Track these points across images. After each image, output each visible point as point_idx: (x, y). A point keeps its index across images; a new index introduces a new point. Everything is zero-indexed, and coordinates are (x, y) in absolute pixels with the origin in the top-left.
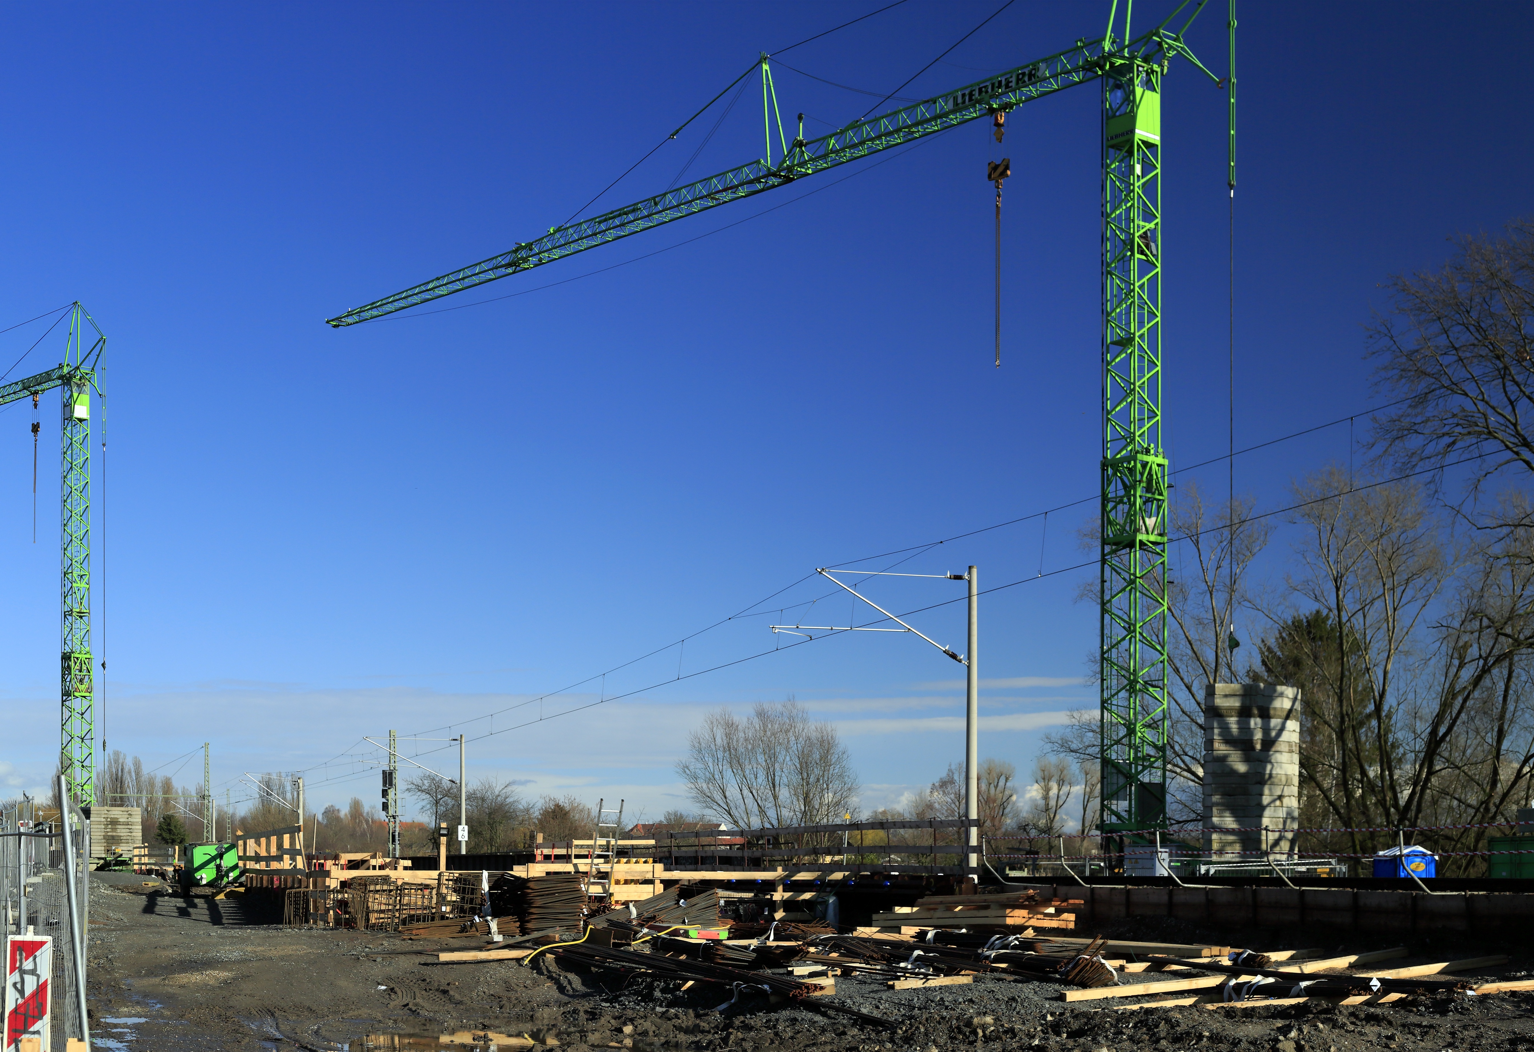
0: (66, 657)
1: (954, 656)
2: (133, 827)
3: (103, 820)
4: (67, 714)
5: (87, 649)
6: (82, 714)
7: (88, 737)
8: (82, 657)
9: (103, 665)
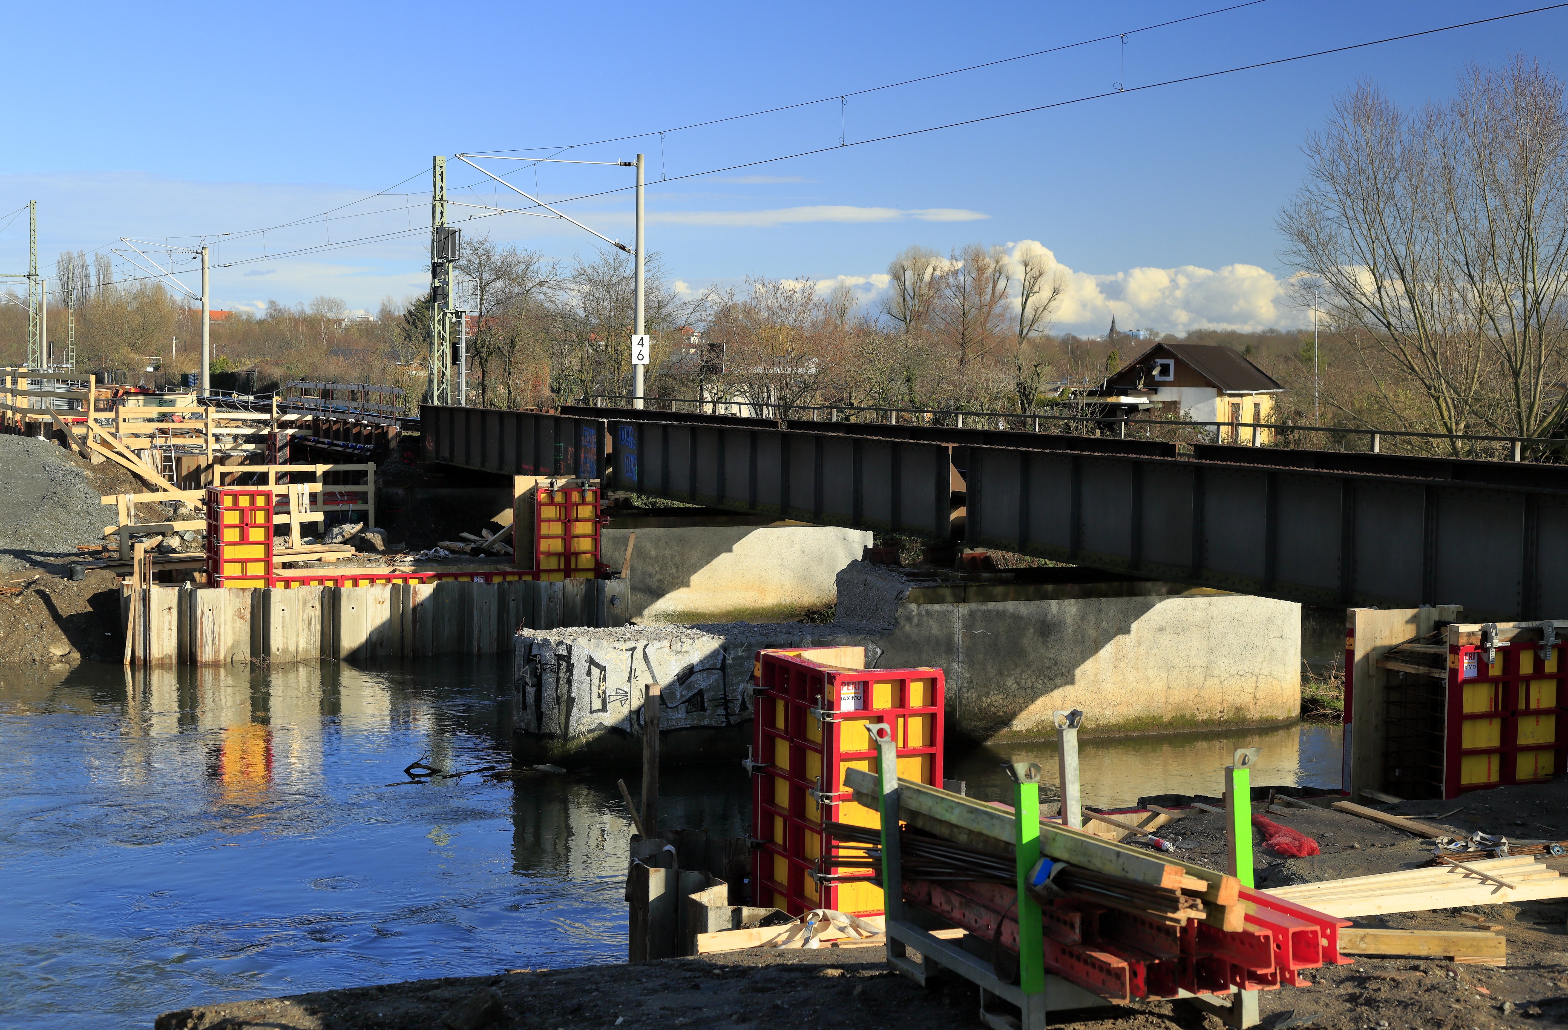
1: (623, 248)
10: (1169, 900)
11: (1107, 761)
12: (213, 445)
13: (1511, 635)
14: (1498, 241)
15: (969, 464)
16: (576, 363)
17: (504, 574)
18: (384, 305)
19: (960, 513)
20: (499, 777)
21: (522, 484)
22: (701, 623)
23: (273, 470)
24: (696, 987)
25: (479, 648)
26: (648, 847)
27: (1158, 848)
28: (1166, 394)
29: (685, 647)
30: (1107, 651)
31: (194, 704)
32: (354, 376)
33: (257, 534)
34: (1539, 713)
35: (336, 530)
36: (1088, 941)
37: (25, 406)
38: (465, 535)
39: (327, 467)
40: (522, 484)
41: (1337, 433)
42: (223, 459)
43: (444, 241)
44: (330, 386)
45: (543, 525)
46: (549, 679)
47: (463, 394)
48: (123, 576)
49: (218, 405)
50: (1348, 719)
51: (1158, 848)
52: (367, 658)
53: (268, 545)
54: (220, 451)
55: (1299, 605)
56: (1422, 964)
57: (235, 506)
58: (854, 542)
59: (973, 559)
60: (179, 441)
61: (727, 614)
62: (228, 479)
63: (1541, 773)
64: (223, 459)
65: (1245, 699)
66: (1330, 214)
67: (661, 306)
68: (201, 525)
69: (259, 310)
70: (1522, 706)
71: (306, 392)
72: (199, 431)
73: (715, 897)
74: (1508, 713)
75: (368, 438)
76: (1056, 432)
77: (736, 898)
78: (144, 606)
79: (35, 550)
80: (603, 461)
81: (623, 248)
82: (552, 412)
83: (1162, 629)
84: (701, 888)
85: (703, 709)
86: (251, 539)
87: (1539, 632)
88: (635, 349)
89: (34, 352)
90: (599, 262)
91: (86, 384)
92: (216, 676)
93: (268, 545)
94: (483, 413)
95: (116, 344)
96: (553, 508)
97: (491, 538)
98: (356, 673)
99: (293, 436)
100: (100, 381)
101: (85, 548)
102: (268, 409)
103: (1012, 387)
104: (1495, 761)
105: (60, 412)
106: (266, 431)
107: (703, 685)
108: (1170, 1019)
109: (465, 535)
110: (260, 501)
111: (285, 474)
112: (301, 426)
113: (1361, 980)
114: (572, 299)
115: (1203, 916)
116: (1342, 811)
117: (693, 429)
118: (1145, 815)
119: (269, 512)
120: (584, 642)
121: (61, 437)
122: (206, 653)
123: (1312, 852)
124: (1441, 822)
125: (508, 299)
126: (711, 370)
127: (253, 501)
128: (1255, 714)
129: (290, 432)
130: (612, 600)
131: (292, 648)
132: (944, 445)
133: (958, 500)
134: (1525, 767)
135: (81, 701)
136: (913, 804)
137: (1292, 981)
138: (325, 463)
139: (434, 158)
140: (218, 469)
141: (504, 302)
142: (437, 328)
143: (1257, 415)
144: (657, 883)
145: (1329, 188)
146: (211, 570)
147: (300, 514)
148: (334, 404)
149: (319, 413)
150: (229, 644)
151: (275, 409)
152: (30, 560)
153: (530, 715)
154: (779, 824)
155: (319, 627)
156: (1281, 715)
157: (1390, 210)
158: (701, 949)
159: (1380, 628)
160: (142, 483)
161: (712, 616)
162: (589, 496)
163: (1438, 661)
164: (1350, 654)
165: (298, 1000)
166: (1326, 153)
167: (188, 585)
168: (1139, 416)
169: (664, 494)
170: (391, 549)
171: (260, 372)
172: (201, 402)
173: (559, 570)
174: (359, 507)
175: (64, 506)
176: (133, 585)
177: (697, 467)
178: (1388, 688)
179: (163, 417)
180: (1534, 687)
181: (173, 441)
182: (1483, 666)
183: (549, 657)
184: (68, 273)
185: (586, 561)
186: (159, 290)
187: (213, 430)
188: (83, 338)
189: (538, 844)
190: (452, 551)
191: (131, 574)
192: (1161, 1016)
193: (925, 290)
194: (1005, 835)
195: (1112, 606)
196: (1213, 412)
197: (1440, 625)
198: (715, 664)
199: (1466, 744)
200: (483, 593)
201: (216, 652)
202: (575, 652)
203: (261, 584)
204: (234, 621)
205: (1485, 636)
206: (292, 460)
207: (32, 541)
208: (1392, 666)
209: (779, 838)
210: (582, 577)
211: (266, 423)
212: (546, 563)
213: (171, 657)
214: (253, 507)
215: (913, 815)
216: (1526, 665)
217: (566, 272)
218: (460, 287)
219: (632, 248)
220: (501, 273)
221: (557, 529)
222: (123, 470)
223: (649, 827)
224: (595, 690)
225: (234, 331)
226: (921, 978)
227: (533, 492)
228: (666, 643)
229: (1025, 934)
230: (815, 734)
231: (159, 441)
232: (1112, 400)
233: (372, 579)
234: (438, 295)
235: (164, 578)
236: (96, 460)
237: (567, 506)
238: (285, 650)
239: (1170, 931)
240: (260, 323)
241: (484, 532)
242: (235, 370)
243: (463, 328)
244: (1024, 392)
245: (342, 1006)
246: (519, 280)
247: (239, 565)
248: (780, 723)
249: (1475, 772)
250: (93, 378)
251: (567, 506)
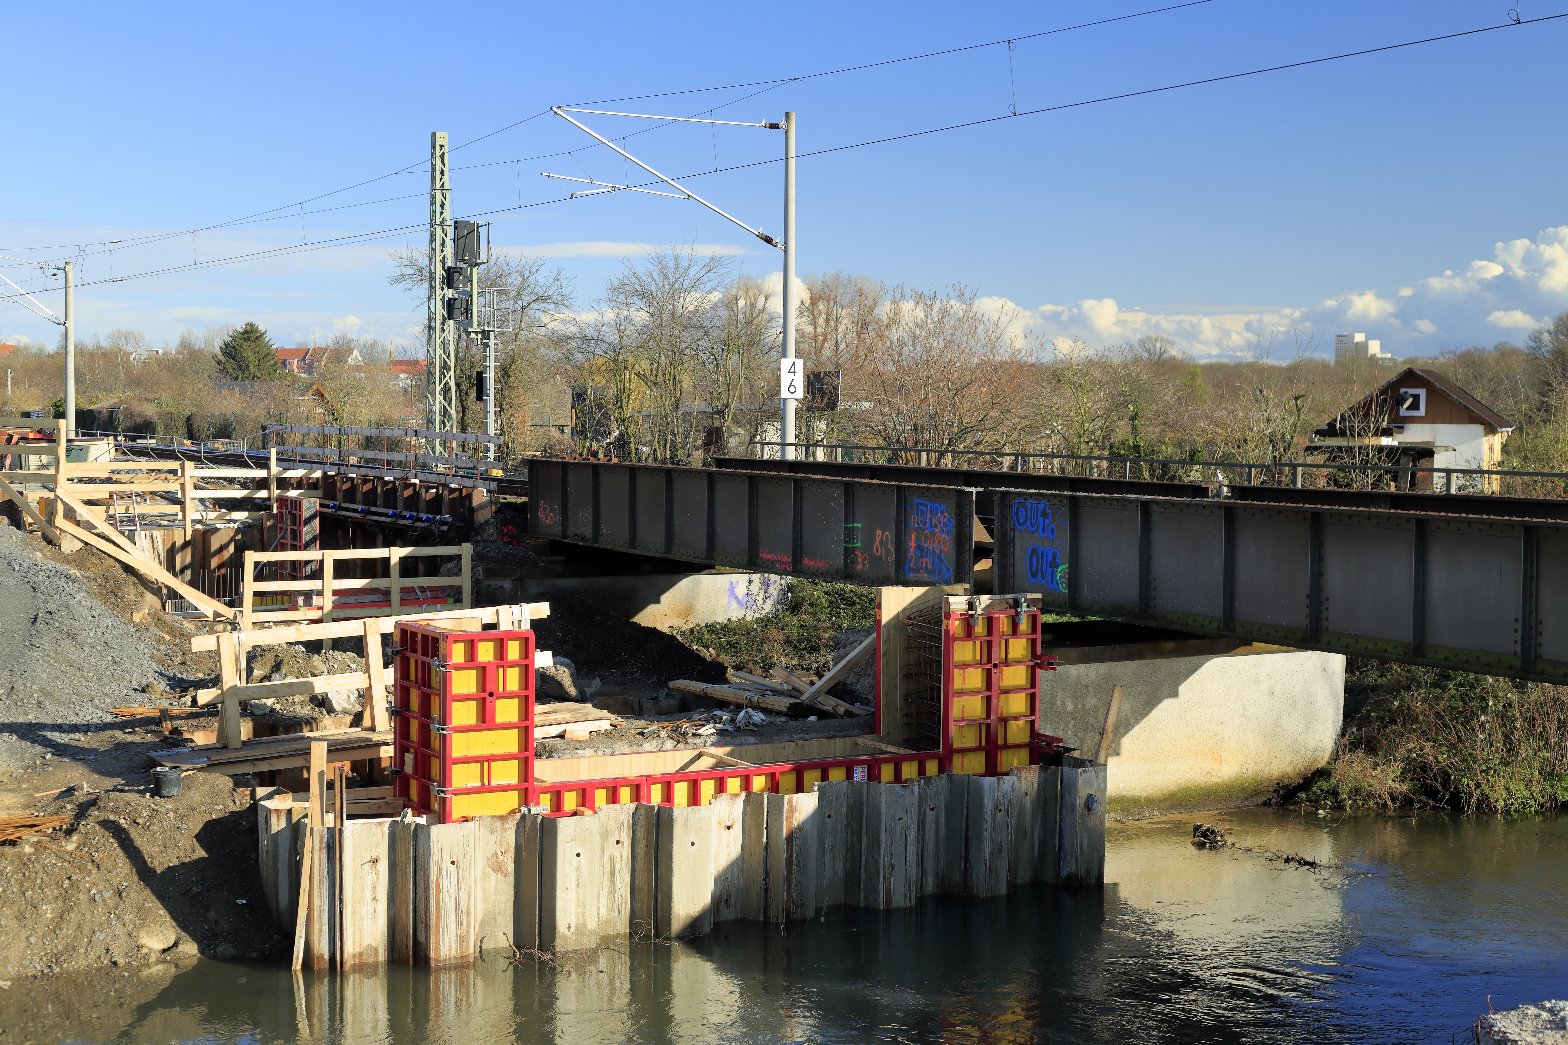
1: (768, 240)
18: (183, 337)
25: (889, 899)
39: (405, 551)
45: (957, 674)
54: (200, 521)
78: (331, 859)
79: (48, 720)
81: (768, 240)
86: (499, 719)
88: (786, 379)
92: (462, 984)
96: (969, 644)
132: (967, 489)
133: (982, 552)
139: (434, 135)
149: (327, 467)
150: (479, 919)
152: (48, 744)
155: (627, 879)
164: (880, 621)
171: (125, 409)
175: (71, 636)
204: (485, 876)
207: (39, 704)
211: (263, 484)
213: (376, 950)
221: (974, 678)
222: (109, 562)
225: (101, 363)
230: (435, 682)
236: (69, 546)
238: (581, 929)
240: (50, 356)
242: (93, 407)
247: (475, 767)
248: (413, 676)
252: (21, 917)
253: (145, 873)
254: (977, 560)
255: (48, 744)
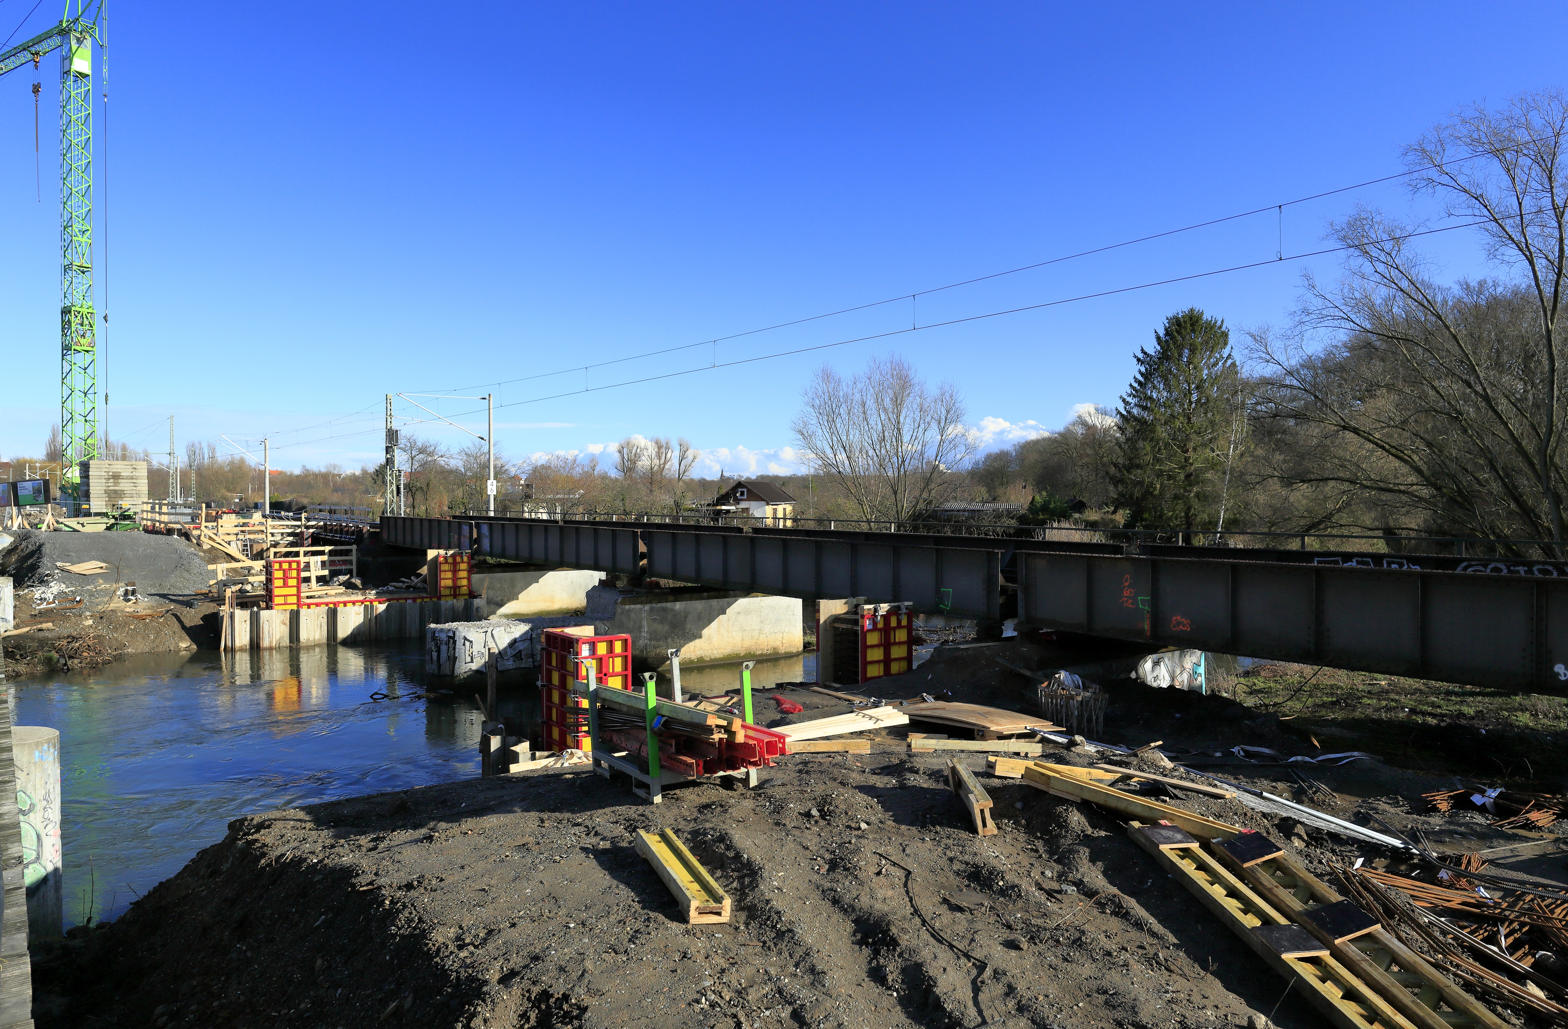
0: (66, 311)
1: (482, 439)
2: (138, 481)
3: (104, 474)
4: (67, 368)
5: (90, 304)
6: (85, 369)
7: (91, 391)
8: (84, 311)
9: (105, 318)
10: (709, 730)
11: (715, 676)
12: (270, 538)
13: (886, 609)
14: (886, 434)
15: (648, 538)
16: (461, 495)
17: (423, 598)
19: (644, 562)
20: (419, 697)
21: (431, 554)
22: (521, 618)
23: (302, 550)
24: (503, 788)
26: (490, 726)
27: (732, 713)
28: (743, 505)
29: (512, 630)
30: (714, 624)
31: (259, 669)
32: (346, 502)
33: (293, 582)
34: (900, 643)
35: (335, 579)
36: (679, 752)
37: (166, 520)
38: (403, 579)
40: (431, 554)
41: (820, 521)
42: (276, 545)
43: (392, 436)
44: (333, 507)
46: (444, 648)
47: (402, 510)
48: (220, 605)
49: (273, 518)
50: (818, 650)
51: (732, 713)
52: (351, 642)
53: (298, 587)
55: (800, 601)
56: (833, 755)
57: (281, 568)
58: (593, 577)
59: (651, 582)
60: (252, 537)
61: (535, 614)
62: (278, 555)
63: (902, 670)
64: (276, 545)
65: (778, 644)
66: (812, 422)
67: (502, 466)
68: (263, 578)
69: (297, 471)
70: (892, 641)
71: (320, 511)
72: (263, 531)
73: (522, 748)
74: (886, 645)
75: (353, 533)
76: (692, 523)
77: (534, 748)
80: (473, 542)
81: (482, 439)
82: (448, 518)
83: (739, 613)
84: (516, 744)
85: (522, 659)
87: (899, 608)
89: (173, 492)
90: (471, 445)
91: (201, 509)
92: (271, 655)
93: (298, 587)
94: (412, 519)
95: (216, 488)
97: (416, 581)
98: (345, 649)
99: (313, 533)
100: (208, 506)
101: (199, 592)
102: (300, 519)
103: (672, 503)
104: (882, 666)
105: (186, 523)
106: (298, 531)
107: (521, 648)
108: (719, 785)
109: (403, 579)
110: (294, 565)
111: (309, 552)
112: (317, 527)
113: (805, 763)
114: (456, 463)
115: (726, 736)
116: (814, 691)
117: (516, 525)
118: (728, 698)
119: (299, 570)
120: (464, 629)
121: (186, 536)
122: (265, 643)
123: (800, 710)
124: (858, 694)
125: (425, 463)
126: (528, 497)
127: (290, 566)
128: (782, 650)
129: (311, 531)
130: (477, 609)
131: (312, 639)
133: (643, 556)
134: (895, 668)
135: (197, 669)
136: (603, 695)
137: (768, 764)
138: (330, 545)
140: (273, 550)
141: (423, 465)
142: (389, 478)
143: (785, 514)
144: (495, 743)
145: (812, 410)
146: (267, 599)
147: (316, 570)
148: (335, 516)
151: (303, 519)
152: (169, 599)
153: (435, 666)
154: (554, 711)
156: (794, 650)
157: (838, 421)
158: (511, 772)
159: (832, 608)
160: (231, 558)
161: (528, 615)
162: (465, 559)
163: (856, 622)
164: (819, 620)
165: (302, 808)
166: (810, 395)
167: (255, 609)
168: (731, 515)
169: (503, 557)
170: (365, 587)
172: (264, 516)
173: (450, 595)
174: (348, 567)
175: (188, 571)
176: (225, 610)
177: (517, 543)
178: (835, 635)
179: (244, 525)
180: (897, 632)
181: (248, 536)
182: (875, 623)
183: (443, 637)
184: (192, 453)
185: (464, 590)
186: (242, 460)
187: (270, 530)
188: (200, 485)
189: (441, 729)
190: (395, 587)
191: (224, 604)
192: (714, 784)
193: (633, 457)
194: (643, 707)
195: (714, 603)
196: (765, 512)
197: (857, 606)
198: (527, 638)
199: (869, 659)
200: (411, 606)
201: (271, 642)
202: (457, 633)
203: (295, 607)
205: (876, 610)
206: (312, 545)
208: (836, 625)
209: (554, 718)
210: (462, 599)
211: (299, 527)
212: (444, 592)
214: (290, 568)
215: (604, 700)
216: (894, 622)
217: (454, 450)
218: (401, 459)
219: (487, 438)
220: (422, 451)
221: (449, 575)
223: (491, 716)
224: (467, 652)
225: (282, 481)
226: (607, 775)
227: (436, 558)
228: (503, 628)
229: (651, 750)
230: (570, 667)
231: (241, 537)
232: (719, 508)
233: (354, 603)
234: (389, 462)
235: (243, 605)
236: (206, 547)
237: (455, 564)
238: (308, 640)
239: (713, 744)
240: (297, 476)
241: (412, 578)
243: (402, 478)
244: (677, 504)
245: (326, 809)
246: (431, 454)
248: (554, 663)
249: (874, 671)
250: (204, 505)
251: (455, 564)
252: (143, 638)
253: (184, 627)
254: (642, 559)
255: (169, 599)
